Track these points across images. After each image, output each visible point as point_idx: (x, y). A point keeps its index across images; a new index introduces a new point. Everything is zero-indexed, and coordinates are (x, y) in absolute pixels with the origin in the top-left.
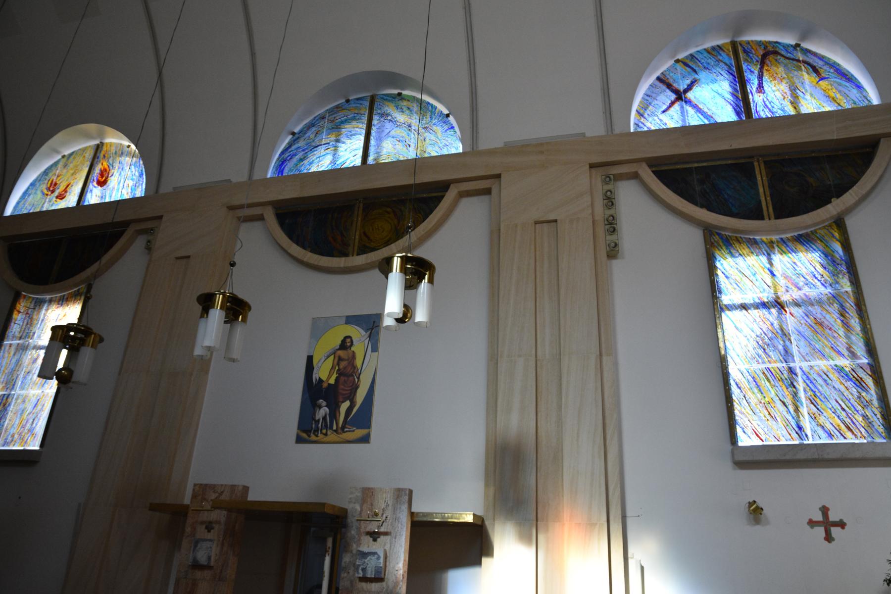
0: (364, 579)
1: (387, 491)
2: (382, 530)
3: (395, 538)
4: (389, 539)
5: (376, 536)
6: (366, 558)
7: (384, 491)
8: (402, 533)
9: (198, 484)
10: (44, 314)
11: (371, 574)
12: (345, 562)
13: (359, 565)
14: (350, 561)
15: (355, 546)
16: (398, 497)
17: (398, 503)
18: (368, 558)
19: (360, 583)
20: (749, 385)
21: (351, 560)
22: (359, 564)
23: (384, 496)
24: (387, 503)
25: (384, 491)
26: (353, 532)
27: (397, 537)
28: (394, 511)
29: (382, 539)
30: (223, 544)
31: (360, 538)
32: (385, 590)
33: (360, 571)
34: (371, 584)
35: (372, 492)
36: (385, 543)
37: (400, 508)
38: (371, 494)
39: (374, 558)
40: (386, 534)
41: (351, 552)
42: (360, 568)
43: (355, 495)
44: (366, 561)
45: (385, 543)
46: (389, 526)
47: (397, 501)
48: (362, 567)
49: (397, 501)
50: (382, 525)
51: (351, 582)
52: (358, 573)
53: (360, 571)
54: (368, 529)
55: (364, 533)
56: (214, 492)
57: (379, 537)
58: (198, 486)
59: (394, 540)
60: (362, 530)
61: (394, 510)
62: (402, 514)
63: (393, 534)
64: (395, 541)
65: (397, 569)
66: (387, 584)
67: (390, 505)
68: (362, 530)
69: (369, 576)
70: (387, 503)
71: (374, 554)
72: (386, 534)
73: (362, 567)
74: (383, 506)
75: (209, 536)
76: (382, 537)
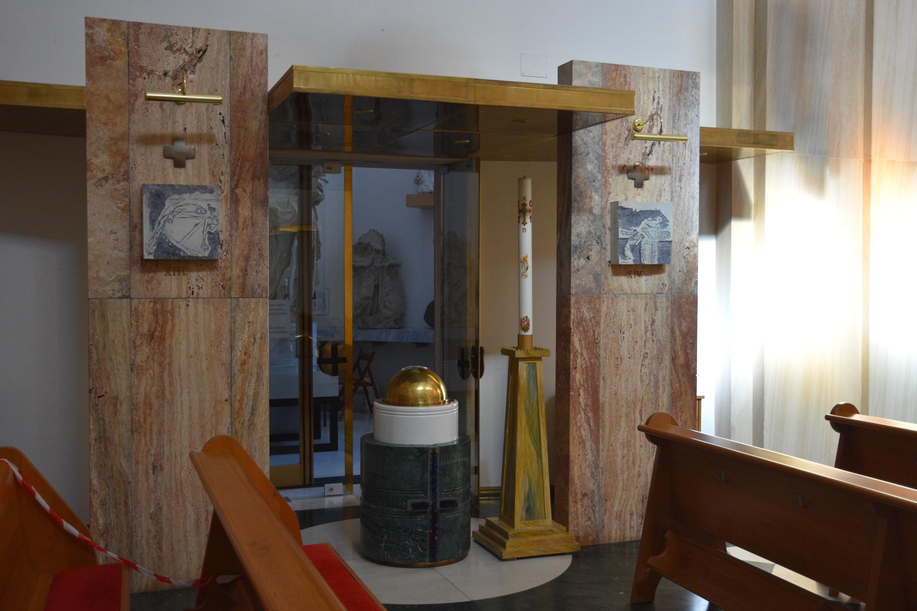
0: (619, 270)
1: (657, 75)
2: (652, 162)
3: (680, 181)
4: (667, 184)
5: (636, 174)
6: (638, 224)
7: (651, 75)
8: (692, 171)
9: (104, 20)
10: (675, 344)
11: (652, 257)
12: (578, 235)
13: (626, 240)
14: (590, 232)
15: (596, 198)
16: (680, 91)
17: (682, 105)
18: (643, 224)
19: (615, 278)
20: (117, 403)
21: (591, 229)
22: (624, 236)
23: (651, 86)
24: (658, 103)
25: (651, 75)
26: (590, 167)
27: (684, 179)
28: (674, 122)
29: (653, 182)
30: (235, 200)
31: (606, 181)
32: (666, 288)
33: (628, 253)
34: (637, 277)
35: (625, 76)
36: (660, 191)
37: (686, 115)
38: (622, 80)
39: (655, 223)
40: (661, 171)
41: (590, 211)
42: (628, 245)
43: (587, 80)
44: (639, 229)
45: (660, 191)
46: (667, 153)
47: (679, 100)
48: (630, 242)
49: (679, 100)
50: (651, 152)
51: (597, 277)
52: (625, 257)
53: (628, 253)
54: (622, 162)
55: (613, 167)
56: (170, 48)
57: (647, 179)
58: (106, 26)
59: (677, 183)
60: (610, 162)
61: (675, 118)
62: (691, 129)
63: (676, 172)
64: (681, 188)
65: (687, 245)
66: (670, 276)
67: (666, 108)
68: (608, 161)
69: (647, 262)
70: (658, 103)
71: (654, 214)
72: (661, 171)
73: (630, 242)
74: (651, 109)
75: (182, 177)
76: (653, 178)
